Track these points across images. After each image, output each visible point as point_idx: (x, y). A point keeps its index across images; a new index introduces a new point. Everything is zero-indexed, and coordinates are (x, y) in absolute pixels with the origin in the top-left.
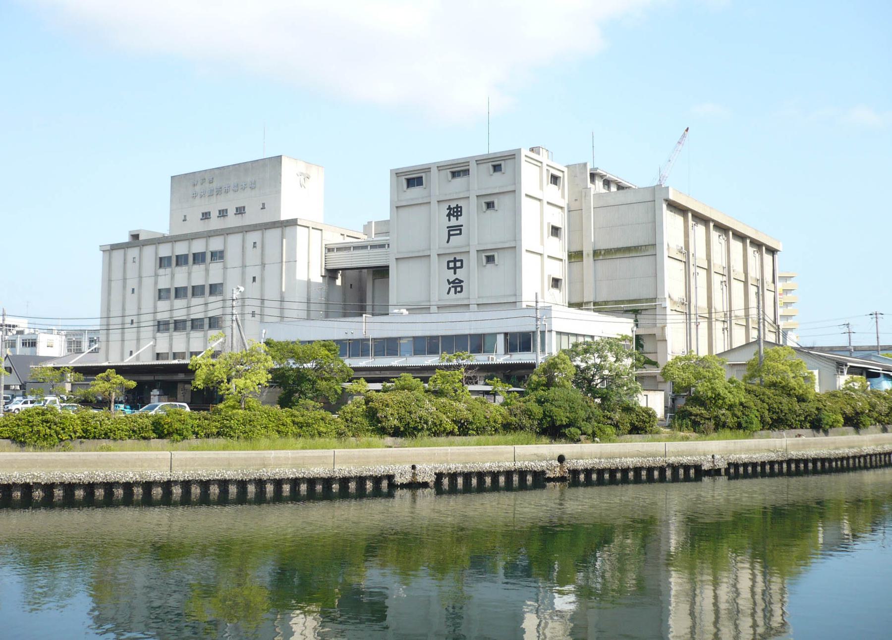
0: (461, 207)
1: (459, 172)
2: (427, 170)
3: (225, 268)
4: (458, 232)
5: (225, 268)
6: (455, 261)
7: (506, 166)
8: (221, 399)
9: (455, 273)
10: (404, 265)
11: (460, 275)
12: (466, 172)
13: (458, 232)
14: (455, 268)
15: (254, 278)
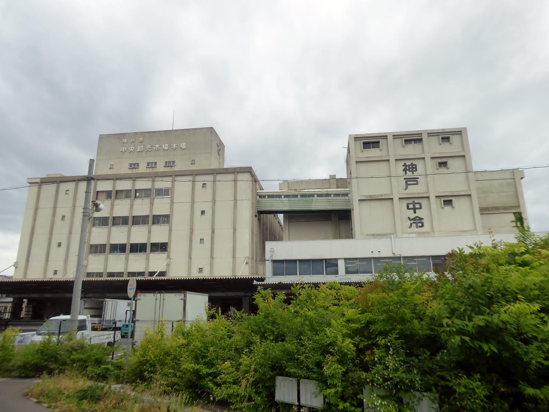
0: (416, 165)
1: (369, 143)
2: (385, 137)
3: (172, 203)
4: (415, 182)
5: (172, 203)
6: (414, 204)
7: (454, 139)
8: (256, 314)
9: (415, 212)
10: (365, 205)
11: (419, 213)
12: (420, 140)
13: (415, 182)
14: (415, 210)
15: (63, 217)
